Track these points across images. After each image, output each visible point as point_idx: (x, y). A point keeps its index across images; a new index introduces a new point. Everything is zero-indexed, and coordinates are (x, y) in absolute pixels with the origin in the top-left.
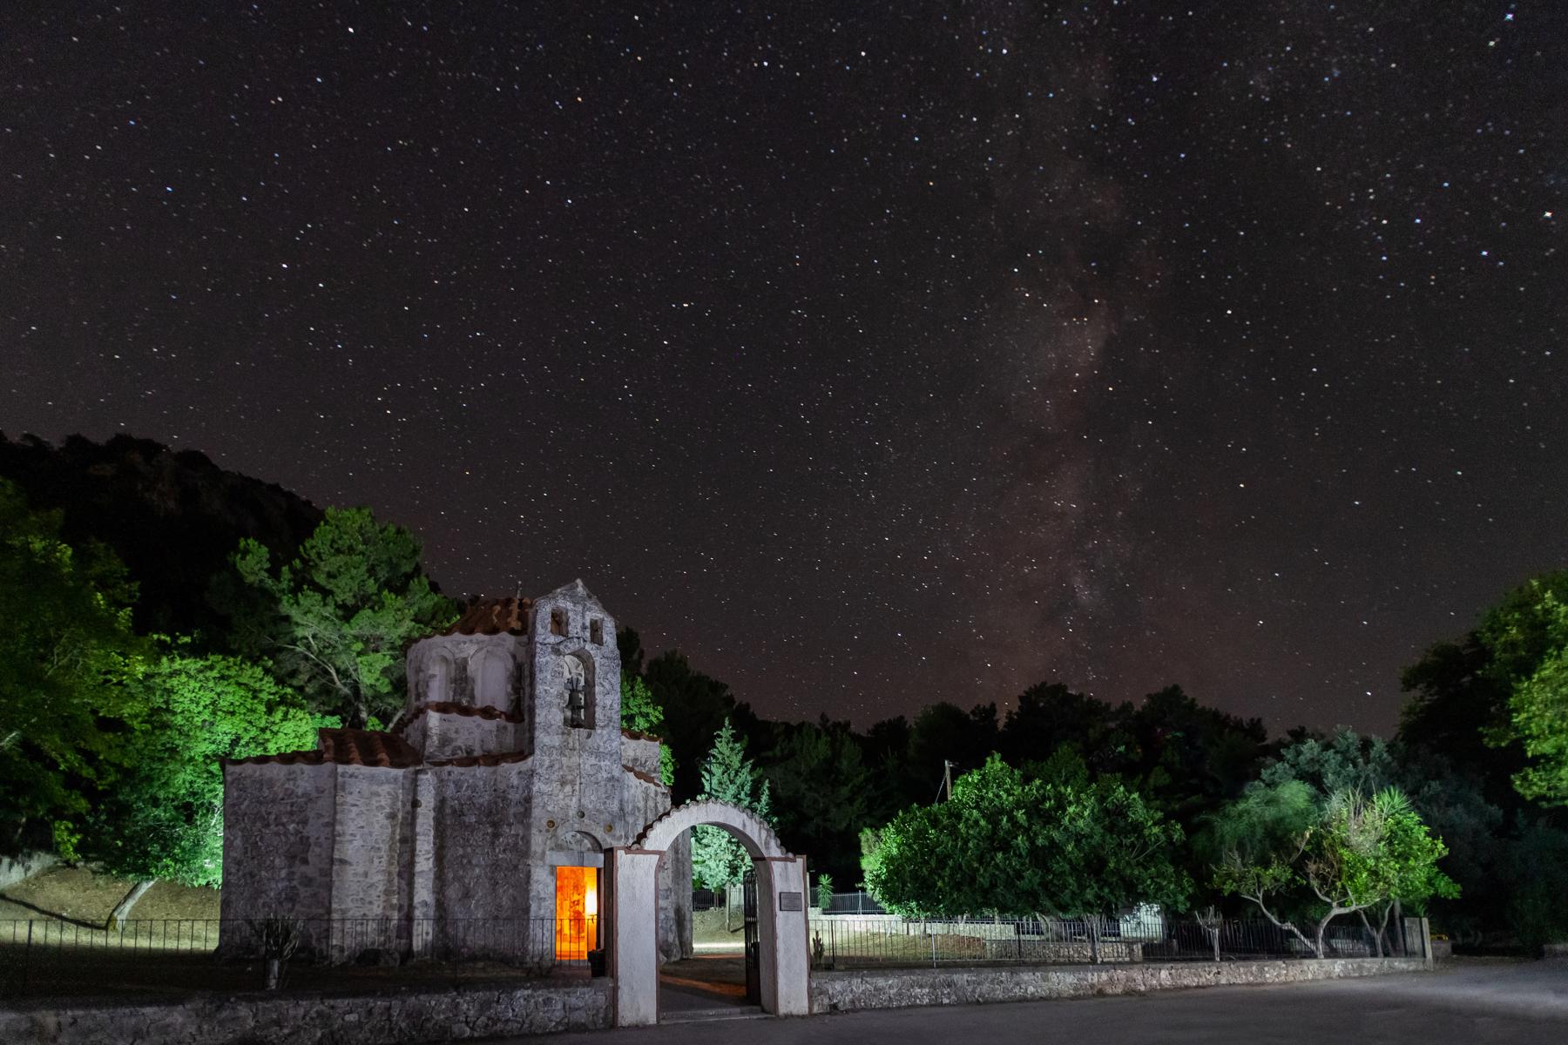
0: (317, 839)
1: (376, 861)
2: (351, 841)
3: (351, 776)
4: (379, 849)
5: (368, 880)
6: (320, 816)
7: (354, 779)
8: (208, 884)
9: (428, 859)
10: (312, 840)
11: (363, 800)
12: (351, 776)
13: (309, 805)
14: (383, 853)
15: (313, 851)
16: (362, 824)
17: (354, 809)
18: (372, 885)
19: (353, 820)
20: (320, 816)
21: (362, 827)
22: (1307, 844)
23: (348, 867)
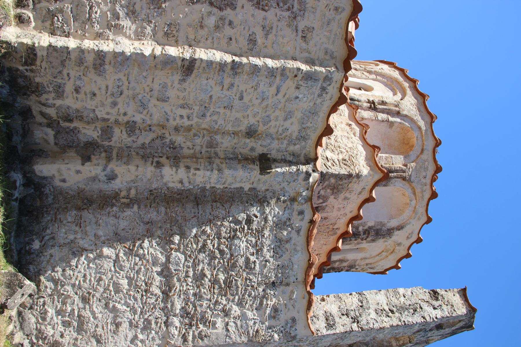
0: (231, 23)
1: (184, 112)
2: (222, 84)
3: (323, 89)
4: (204, 115)
5: (154, 101)
6: (267, 30)
7: (318, 92)
8: (224, 71)
9: (181, 182)
10: (228, 12)
11: (283, 100)
12: (323, 89)
13: (287, 14)
14: (196, 120)
15: (210, 13)
16: (246, 99)
17: (273, 89)
18: (143, 105)
19: (255, 88)
20: (267, 30)
21: (241, 98)
22: (75, 333)
23: (177, 77)
